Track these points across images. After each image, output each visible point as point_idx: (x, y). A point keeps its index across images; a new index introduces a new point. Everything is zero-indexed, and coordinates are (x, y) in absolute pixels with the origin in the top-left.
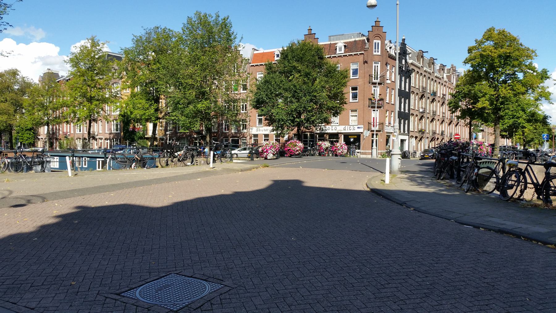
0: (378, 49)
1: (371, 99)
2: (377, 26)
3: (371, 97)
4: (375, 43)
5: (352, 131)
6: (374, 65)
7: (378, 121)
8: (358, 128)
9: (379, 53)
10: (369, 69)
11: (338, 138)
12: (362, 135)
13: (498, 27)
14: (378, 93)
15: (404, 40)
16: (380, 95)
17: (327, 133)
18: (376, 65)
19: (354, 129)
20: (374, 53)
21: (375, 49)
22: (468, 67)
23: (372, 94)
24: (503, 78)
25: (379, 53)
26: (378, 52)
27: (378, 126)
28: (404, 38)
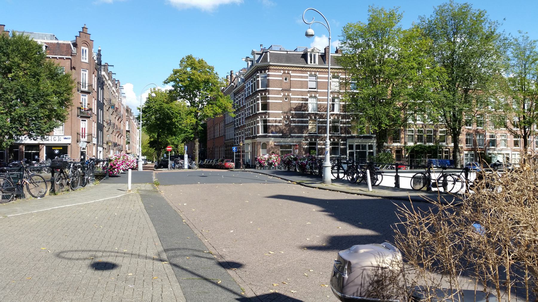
0: (86, 56)
1: (80, 108)
2: (84, 32)
3: (80, 106)
4: (83, 50)
5: (57, 142)
6: (82, 72)
7: (86, 132)
8: (65, 138)
9: (87, 61)
10: (77, 76)
11: (40, 150)
12: (69, 147)
13: (197, 56)
14: (87, 103)
15: (99, 51)
16: (88, 104)
17: (23, 144)
18: (84, 72)
19: (59, 140)
20: (82, 60)
21: (83, 55)
22: (170, 87)
23: (81, 103)
24: (493, 100)
25: (87, 61)
26: (86, 59)
27: (86, 137)
28: (100, 49)
